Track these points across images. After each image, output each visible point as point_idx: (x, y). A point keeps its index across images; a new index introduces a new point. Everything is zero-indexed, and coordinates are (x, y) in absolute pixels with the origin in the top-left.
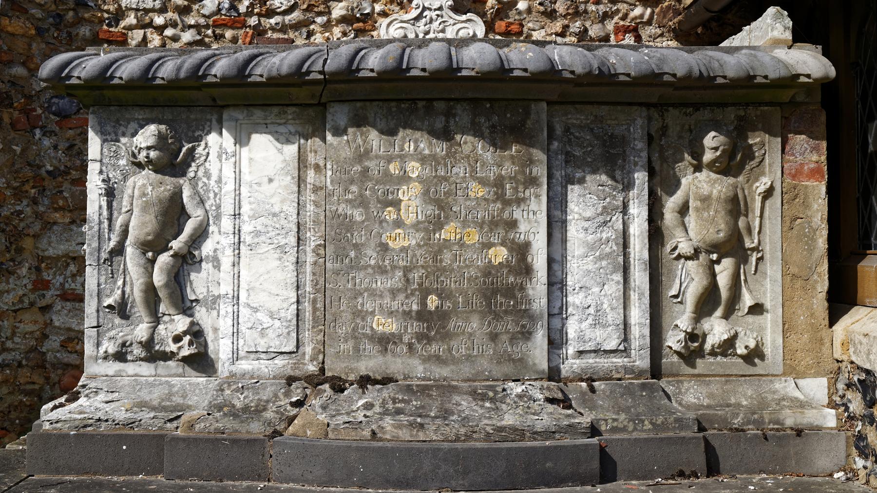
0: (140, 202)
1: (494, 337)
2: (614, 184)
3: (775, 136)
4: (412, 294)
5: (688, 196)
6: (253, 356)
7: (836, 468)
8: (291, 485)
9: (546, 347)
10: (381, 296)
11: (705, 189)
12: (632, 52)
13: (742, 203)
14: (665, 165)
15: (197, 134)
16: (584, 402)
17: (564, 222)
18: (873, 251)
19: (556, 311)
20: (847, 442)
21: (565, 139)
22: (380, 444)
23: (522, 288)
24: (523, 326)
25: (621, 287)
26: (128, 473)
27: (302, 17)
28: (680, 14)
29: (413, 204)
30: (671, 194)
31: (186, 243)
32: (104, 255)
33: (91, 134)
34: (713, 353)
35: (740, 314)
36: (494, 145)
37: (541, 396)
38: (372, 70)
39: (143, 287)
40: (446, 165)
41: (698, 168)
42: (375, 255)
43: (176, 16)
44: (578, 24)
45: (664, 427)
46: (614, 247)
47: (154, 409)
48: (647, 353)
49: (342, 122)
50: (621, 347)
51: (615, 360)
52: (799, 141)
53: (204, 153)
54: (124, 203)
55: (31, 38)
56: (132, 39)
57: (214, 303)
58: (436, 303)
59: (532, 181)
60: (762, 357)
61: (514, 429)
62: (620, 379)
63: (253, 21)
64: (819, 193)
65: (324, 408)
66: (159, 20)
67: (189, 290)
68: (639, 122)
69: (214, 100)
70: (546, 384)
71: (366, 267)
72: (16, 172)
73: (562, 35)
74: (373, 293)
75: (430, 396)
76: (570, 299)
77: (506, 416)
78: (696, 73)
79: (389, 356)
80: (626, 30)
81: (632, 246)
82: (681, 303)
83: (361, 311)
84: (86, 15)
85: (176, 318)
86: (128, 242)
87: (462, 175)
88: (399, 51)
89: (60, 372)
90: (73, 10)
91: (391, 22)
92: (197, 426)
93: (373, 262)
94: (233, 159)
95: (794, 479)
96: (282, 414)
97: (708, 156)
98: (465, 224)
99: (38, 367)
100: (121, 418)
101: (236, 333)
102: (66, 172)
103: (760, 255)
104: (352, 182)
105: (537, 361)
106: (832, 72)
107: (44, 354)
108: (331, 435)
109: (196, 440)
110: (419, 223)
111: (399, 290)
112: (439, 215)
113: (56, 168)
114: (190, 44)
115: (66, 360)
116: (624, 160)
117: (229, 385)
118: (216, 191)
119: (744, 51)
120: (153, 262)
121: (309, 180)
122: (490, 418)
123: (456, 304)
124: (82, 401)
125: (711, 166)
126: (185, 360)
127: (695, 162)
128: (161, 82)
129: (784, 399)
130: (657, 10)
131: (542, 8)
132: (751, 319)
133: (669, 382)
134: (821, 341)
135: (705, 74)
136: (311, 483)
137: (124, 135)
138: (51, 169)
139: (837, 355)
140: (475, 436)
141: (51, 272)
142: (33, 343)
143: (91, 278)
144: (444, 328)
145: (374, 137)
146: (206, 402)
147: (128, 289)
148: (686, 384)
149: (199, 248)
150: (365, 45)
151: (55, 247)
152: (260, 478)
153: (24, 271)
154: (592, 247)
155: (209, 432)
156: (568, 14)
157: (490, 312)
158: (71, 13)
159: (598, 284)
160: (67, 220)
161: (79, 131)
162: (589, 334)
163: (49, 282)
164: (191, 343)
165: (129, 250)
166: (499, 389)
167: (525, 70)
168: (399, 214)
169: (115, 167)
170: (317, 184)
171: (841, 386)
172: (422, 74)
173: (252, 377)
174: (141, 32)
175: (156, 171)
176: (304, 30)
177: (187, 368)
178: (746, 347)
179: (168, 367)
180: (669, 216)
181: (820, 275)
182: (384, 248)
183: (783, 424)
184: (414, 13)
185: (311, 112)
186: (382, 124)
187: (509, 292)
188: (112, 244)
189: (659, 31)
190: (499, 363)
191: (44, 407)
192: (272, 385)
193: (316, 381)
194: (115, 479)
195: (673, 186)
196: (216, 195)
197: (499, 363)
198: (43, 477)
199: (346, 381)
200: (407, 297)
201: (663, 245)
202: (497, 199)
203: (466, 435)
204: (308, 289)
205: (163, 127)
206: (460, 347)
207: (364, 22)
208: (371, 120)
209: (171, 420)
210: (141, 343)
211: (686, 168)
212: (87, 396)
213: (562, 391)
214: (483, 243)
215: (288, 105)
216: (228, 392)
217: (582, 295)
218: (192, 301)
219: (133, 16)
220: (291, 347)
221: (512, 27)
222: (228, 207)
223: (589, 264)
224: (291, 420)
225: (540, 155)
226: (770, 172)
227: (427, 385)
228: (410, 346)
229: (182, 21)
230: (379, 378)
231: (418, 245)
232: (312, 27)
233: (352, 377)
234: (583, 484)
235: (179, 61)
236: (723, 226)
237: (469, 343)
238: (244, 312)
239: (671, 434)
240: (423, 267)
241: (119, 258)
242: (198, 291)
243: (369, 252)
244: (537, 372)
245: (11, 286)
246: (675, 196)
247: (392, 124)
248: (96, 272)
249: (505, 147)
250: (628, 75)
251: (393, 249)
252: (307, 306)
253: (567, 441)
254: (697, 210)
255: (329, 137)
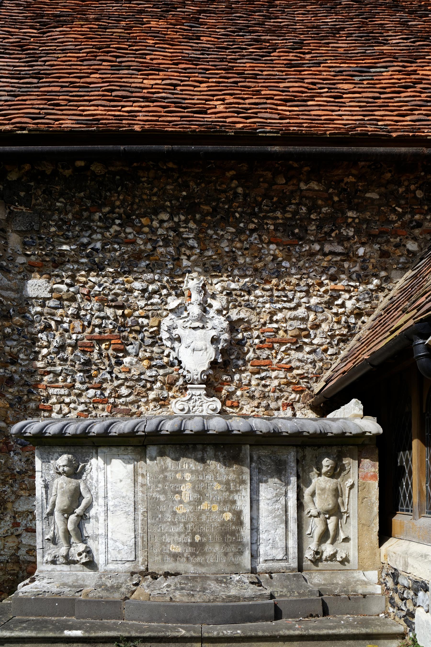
0: (60, 491)
1: (226, 554)
2: (281, 482)
3: (355, 460)
4: (188, 534)
5: (315, 488)
6: (115, 562)
7: (381, 612)
8: (134, 622)
9: (250, 558)
10: (174, 535)
11: (323, 485)
12: (289, 421)
13: (340, 491)
14: (304, 474)
15: (86, 459)
16: (267, 583)
17: (258, 501)
18: (399, 512)
19: (254, 542)
20: (386, 600)
21: (258, 462)
22: (174, 604)
23: (239, 532)
24: (239, 549)
25: (284, 530)
26: (59, 616)
27: (135, 399)
28: (313, 398)
29: (188, 493)
30: (307, 487)
31: (82, 510)
32: (45, 516)
33: (37, 459)
34: (326, 560)
35: (339, 542)
36: (225, 465)
37: (248, 581)
38: (167, 431)
39: (63, 530)
40: (203, 475)
41: (320, 475)
42: (170, 516)
43: (75, 398)
44: (265, 402)
45: (303, 594)
46: (281, 512)
47: (70, 586)
48: (296, 560)
49: (154, 454)
50: (285, 558)
51: (281, 564)
52: (366, 462)
53: (90, 468)
54: (53, 491)
55: (7, 408)
56: (55, 409)
57: (96, 538)
58: (199, 539)
59: (243, 482)
60: (348, 561)
61: (235, 597)
62: (284, 573)
63: (112, 400)
64: (375, 486)
65: (148, 586)
66: (67, 400)
67: (84, 532)
68: (293, 453)
69: (94, 443)
70: (250, 575)
71: (166, 522)
72: (3, 472)
73: (258, 407)
74: (170, 534)
75: (196, 581)
76: (261, 536)
77: (232, 590)
78: (319, 431)
79: (178, 563)
80: (288, 405)
81: (289, 511)
82: (312, 537)
83: (164, 542)
84: (33, 398)
85: (79, 544)
86: (55, 510)
87: (210, 479)
88: (180, 422)
89: (26, 565)
90: (27, 395)
91: (177, 401)
92: (90, 595)
93: (169, 520)
94: (103, 471)
95: (362, 617)
96: (129, 589)
97: (324, 470)
98: (212, 502)
99: (16, 562)
100: (55, 591)
101: (107, 552)
102: (26, 472)
103: (348, 515)
104: (159, 482)
105: (246, 565)
106: (381, 431)
107: (19, 556)
108: (151, 599)
109: (89, 601)
110: (190, 501)
111: (182, 533)
112: (200, 498)
113: (21, 470)
114: (82, 411)
115: (29, 559)
116: (286, 472)
117: (104, 576)
118: (96, 485)
119: (341, 420)
120: (67, 519)
121: (139, 481)
122: (224, 591)
123: (208, 539)
124: (36, 582)
125: (326, 474)
126: (84, 564)
127: (318, 472)
128: (69, 435)
129: (358, 581)
130: (302, 395)
131: (248, 395)
132: (343, 544)
133: (306, 573)
134: (375, 554)
135: (323, 432)
136: (143, 621)
137: (52, 459)
138: (19, 470)
139: (382, 561)
140: (217, 600)
141: (21, 518)
142: (13, 551)
143: (39, 526)
144: (203, 550)
145: (169, 461)
146: (94, 584)
147: (56, 531)
148: (314, 574)
149: (89, 512)
150: (164, 418)
151: (21, 507)
152: (119, 618)
153: (8, 518)
154: (271, 512)
155: (96, 598)
156: (260, 397)
157: (224, 542)
158: (26, 397)
159: (274, 529)
160: (27, 494)
161: (31, 453)
162: (269, 552)
163: (19, 523)
164: (86, 556)
165: (56, 513)
166: (229, 578)
167: (239, 431)
168: (181, 498)
169: (48, 474)
170: (143, 483)
171: (384, 574)
172: (191, 433)
173: (115, 572)
174: (59, 405)
175: (68, 476)
176: (136, 405)
177: (84, 567)
178: (341, 557)
179: (76, 567)
180: (306, 497)
181: (375, 524)
182: (175, 513)
183: (357, 592)
184: (188, 397)
185: (139, 449)
186: (173, 455)
187: (233, 533)
188: (48, 510)
189: (303, 405)
190: (228, 566)
191: (19, 585)
192: (124, 576)
193: (144, 574)
194: (53, 618)
195: (308, 483)
196: (96, 487)
197: (228, 566)
198: (20, 617)
199: (158, 574)
200: (185, 536)
201: (304, 511)
202: (227, 490)
203: (213, 599)
204: (140, 531)
205: (70, 456)
206: (210, 559)
207: (164, 401)
208: (167, 453)
209: (78, 592)
210: (63, 556)
211: (314, 475)
212: (39, 580)
213: (257, 578)
214: (220, 511)
215: (128, 446)
216: (104, 579)
217: (266, 534)
218: (86, 537)
219: (55, 398)
220: (132, 558)
221: (234, 403)
222: (101, 494)
223: (269, 520)
224: (133, 592)
225: (246, 470)
226: (353, 477)
227: (195, 576)
228: (187, 558)
229: (78, 400)
230: (173, 573)
231: (191, 512)
232: (140, 403)
233: (161, 572)
234: (267, 621)
235: (77, 425)
236: (331, 502)
237: (214, 557)
238: (110, 542)
239: (306, 598)
240: (193, 522)
241: (52, 517)
242: (89, 532)
243: (168, 515)
244: (246, 570)
245: (2, 525)
246: (309, 488)
247: (177, 455)
248: (41, 523)
249: (230, 466)
250: (287, 432)
251: (179, 514)
252: (139, 540)
253: (260, 602)
254: (319, 494)
255: (148, 461)
